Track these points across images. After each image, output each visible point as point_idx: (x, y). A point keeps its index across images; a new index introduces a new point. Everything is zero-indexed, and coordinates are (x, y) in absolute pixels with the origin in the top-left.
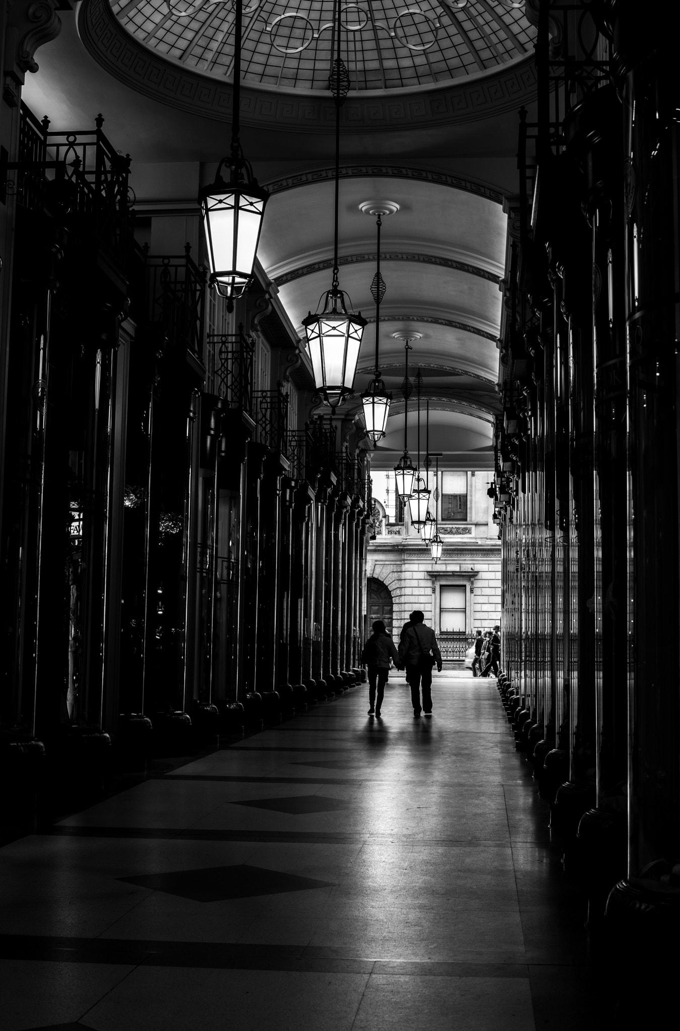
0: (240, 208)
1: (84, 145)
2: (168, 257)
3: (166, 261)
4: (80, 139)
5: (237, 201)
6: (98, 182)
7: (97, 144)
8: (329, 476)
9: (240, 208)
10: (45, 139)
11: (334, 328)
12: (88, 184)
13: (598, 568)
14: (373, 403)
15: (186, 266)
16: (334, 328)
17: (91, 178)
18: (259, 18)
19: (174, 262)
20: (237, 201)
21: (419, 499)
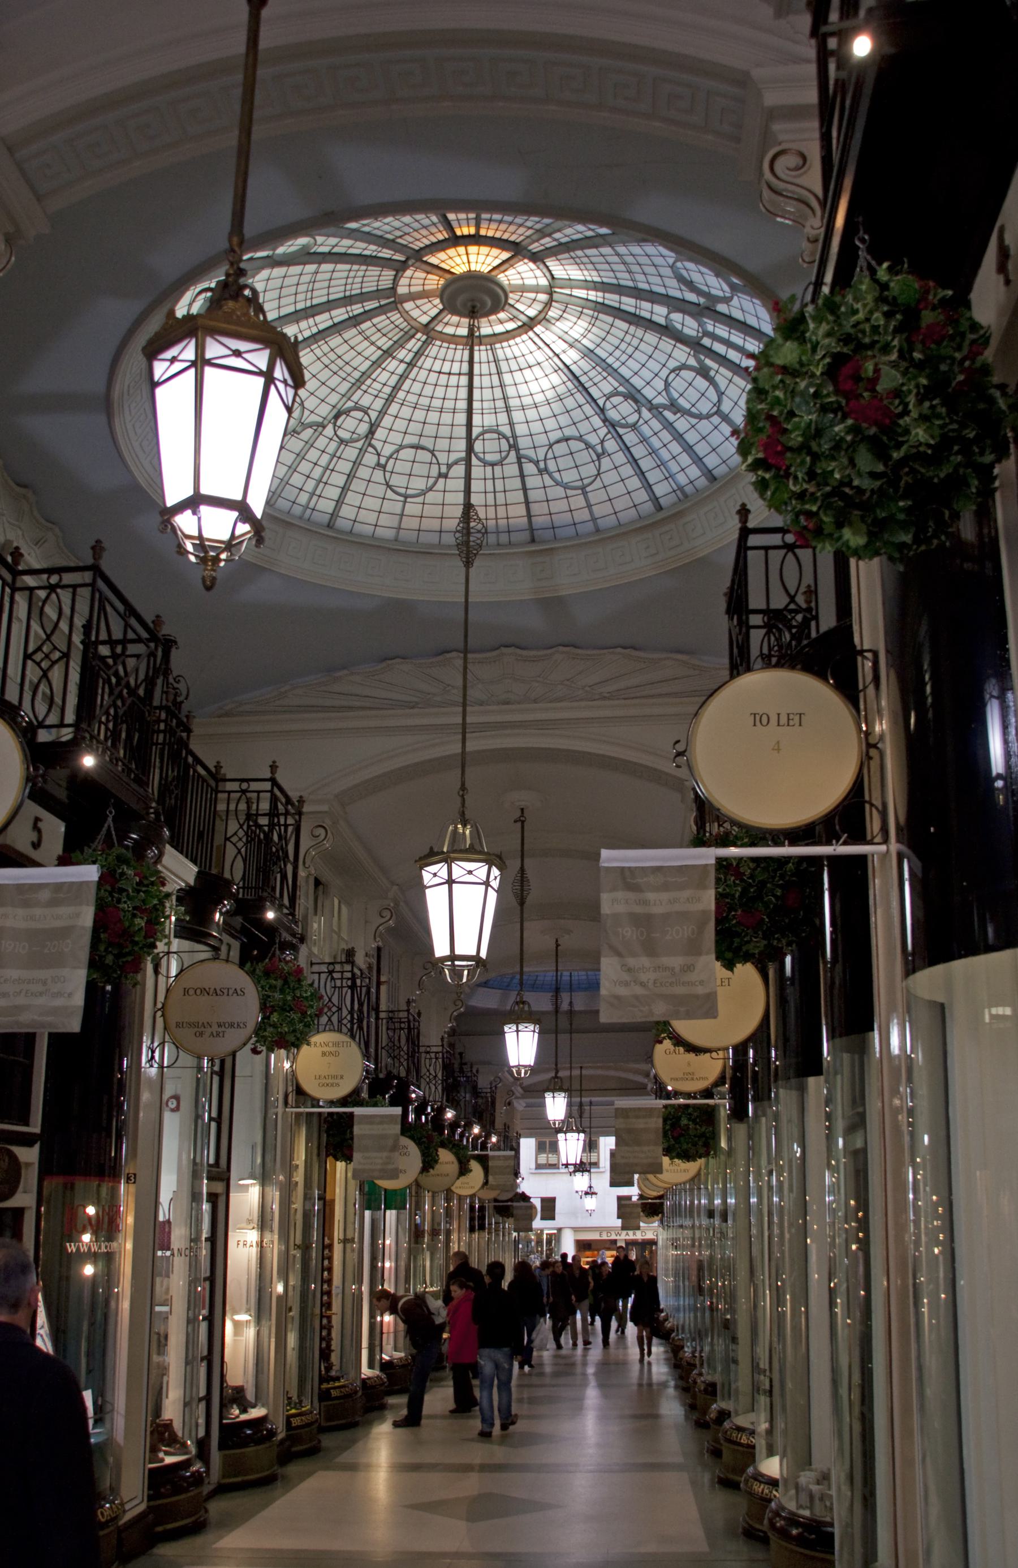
0: (209, 363)
1: (74, 587)
2: (247, 780)
3: (244, 786)
4: (68, 578)
5: (200, 350)
6: (272, 826)
7: (271, 791)
8: (13, 560)
9: (209, 363)
10: (217, 786)
11: (470, 872)
12: (260, 827)
13: (837, 983)
14: (518, 1031)
15: (93, 584)
16: (470, 872)
17: (264, 821)
18: (609, 436)
19: (254, 786)
20: (200, 350)
21: (450, 882)
